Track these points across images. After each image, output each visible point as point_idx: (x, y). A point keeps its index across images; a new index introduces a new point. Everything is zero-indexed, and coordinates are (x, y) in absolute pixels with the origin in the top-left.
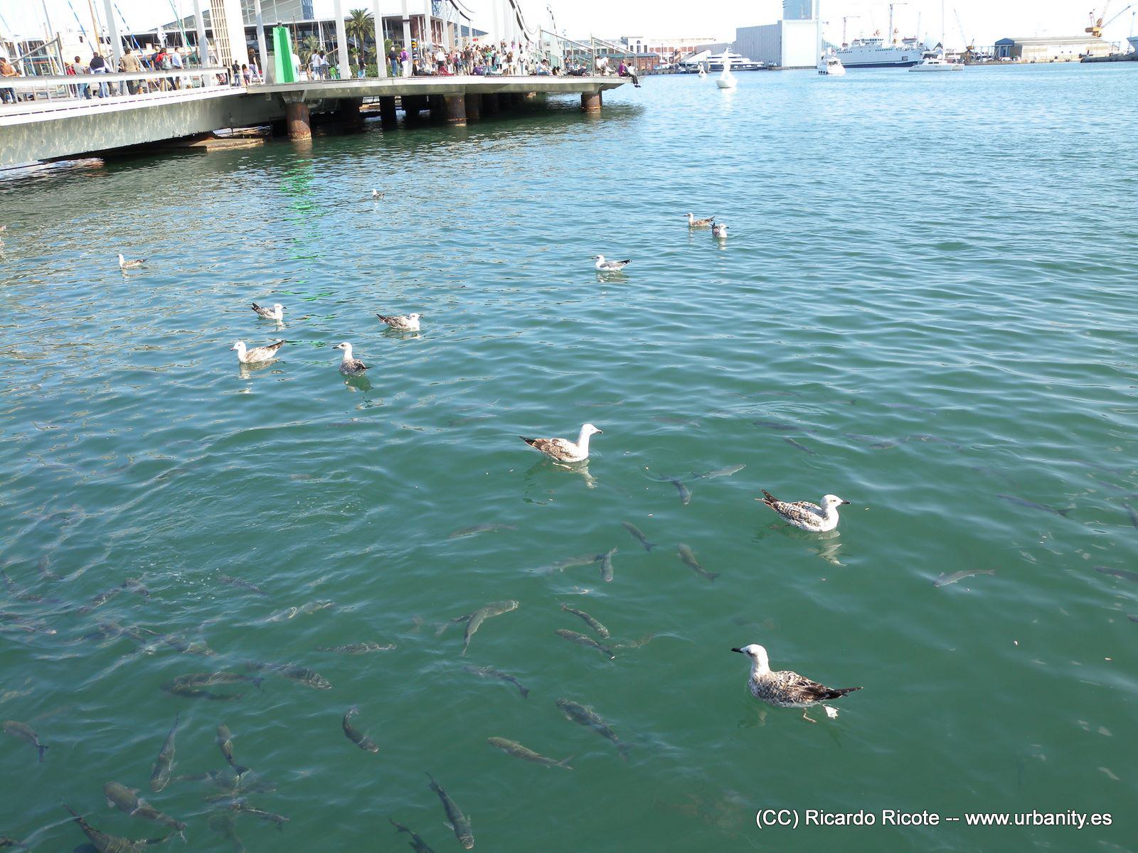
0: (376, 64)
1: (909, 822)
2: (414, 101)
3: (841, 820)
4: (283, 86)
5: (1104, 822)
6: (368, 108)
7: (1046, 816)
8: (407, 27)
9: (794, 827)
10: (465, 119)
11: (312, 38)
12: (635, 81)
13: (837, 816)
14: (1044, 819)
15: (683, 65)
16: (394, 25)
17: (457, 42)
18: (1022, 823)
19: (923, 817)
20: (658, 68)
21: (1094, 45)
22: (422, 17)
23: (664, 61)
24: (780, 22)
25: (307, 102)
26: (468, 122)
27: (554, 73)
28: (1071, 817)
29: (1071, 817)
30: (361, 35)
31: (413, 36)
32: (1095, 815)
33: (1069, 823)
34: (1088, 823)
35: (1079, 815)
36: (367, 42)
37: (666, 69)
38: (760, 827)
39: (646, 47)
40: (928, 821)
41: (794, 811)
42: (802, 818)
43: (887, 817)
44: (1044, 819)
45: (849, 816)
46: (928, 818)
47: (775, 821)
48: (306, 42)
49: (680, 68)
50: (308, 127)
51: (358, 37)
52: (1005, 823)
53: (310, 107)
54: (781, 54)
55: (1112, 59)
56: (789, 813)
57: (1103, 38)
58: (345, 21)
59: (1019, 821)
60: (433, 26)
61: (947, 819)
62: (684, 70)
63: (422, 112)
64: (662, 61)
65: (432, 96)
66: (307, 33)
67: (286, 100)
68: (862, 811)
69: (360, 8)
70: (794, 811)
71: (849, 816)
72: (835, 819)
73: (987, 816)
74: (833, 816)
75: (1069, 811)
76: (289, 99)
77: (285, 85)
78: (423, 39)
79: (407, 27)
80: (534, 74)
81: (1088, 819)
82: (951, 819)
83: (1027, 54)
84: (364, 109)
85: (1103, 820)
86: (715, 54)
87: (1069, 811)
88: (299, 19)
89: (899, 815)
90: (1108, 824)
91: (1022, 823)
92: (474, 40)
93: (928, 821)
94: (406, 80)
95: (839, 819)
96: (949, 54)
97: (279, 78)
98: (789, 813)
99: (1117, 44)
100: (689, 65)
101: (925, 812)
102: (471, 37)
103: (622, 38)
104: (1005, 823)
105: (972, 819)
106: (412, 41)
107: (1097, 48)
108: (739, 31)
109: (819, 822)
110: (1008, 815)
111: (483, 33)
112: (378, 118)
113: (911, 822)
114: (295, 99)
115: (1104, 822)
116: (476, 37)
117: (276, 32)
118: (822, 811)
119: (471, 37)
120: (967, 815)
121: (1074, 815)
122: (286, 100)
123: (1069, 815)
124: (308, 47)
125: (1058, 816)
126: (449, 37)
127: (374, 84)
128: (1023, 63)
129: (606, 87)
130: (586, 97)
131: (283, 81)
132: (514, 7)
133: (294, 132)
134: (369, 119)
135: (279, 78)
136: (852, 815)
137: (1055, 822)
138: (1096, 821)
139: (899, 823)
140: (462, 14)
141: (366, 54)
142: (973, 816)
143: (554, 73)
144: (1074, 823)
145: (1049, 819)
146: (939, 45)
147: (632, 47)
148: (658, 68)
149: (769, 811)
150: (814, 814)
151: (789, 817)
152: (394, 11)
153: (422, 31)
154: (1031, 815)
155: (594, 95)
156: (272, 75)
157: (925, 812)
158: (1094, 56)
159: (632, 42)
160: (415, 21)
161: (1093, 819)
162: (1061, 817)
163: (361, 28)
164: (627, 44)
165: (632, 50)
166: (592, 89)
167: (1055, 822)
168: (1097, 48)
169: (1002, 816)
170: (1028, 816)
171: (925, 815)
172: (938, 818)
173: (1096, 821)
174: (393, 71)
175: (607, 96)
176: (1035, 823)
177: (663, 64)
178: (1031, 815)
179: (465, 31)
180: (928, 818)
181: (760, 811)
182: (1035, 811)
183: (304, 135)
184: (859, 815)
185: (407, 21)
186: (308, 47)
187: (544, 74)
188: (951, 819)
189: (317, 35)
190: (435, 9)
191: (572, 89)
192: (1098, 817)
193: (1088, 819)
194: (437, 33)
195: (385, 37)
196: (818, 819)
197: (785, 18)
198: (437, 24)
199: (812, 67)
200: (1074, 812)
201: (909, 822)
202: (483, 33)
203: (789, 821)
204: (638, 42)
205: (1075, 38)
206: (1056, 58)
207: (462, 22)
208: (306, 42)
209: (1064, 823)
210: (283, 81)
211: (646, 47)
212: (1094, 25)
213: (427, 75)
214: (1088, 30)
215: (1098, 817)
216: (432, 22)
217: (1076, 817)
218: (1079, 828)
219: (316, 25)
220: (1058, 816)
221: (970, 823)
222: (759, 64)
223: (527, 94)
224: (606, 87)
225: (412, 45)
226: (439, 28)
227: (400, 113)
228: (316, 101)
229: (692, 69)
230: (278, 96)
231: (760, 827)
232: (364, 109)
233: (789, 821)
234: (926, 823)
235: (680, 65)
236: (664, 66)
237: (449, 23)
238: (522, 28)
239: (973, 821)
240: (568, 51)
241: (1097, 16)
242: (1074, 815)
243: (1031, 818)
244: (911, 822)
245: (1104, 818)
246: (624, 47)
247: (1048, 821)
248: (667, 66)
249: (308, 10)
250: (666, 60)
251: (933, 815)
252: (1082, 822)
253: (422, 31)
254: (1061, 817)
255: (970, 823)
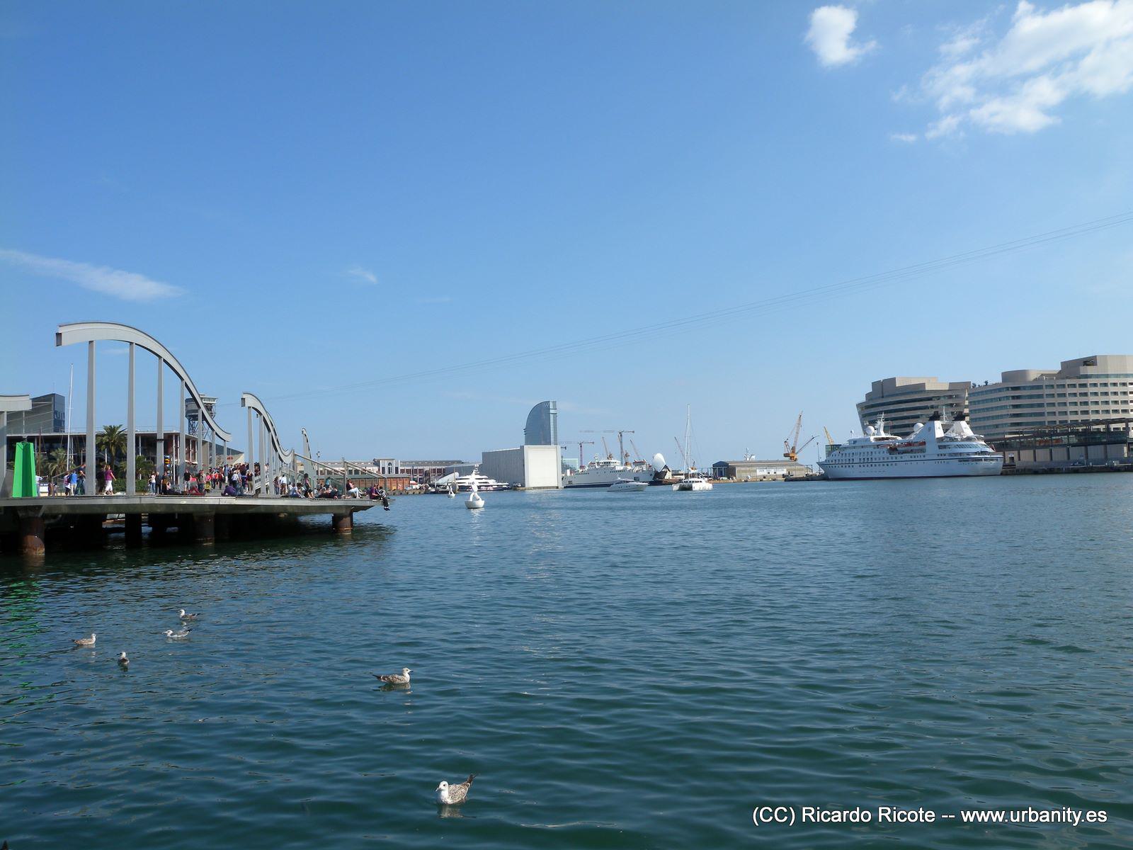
0: (125, 478)
1: (905, 819)
2: (161, 519)
3: (838, 817)
4: (20, 501)
5: (1099, 819)
6: (113, 523)
7: (1041, 813)
8: (160, 447)
9: (791, 825)
10: (214, 538)
11: (60, 450)
12: (385, 503)
13: (833, 813)
14: (1040, 816)
15: (433, 486)
16: (147, 442)
17: (211, 460)
18: (1018, 820)
19: (919, 814)
20: (409, 489)
21: (793, 467)
22: (177, 435)
23: (414, 482)
24: (522, 448)
25: (45, 517)
26: (216, 541)
27: (306, 495)
28: (1066, 814)
29: (1066, 814)
30: (113, 449)
31: (166, 452)
32: (1090, 812)
33: (1064, 821)
34: (1083, 821)
35: (1074, 812)
36: (119, 457)
37: (417, 489)
38: (757, 825)
39: (397, 469)
40: (924, 818)
41: (791, 808)
42: (799, 814)
43: (883, 814)
44: (1040, 816)
45: (845, 813)
46: (924, 815)
47: (771, 818)
48: (53, 454)
49: (430, 488)
50: (41, 542)
51: (110, 451)
52: (1001, 820)
53: (47, 522)
54: (524, 465)
55: (809, 478)
56: (785, 810)
57: (798, 462)
58: (97, 436)
59: (1015, 818)
60: (188, 445)
61: (943, 816)
62: (433, 490)
63: (170, 529)
64: (411, 482)
65: (180, 515)
66: (55, 445)
67: (21, 514)
68: (858, 808)
69: (115, 424)
70: (791, 808)
71: (845, 813)
72: (831, 816)
73: (983, 813)
74: (829, 813)
75: (1064, 808)
76: (24, 514)
77: (21, 499)
78: (176, 456)
79: (160, 447)
80: (286, 497)
81: (1083, 816)
82: (947, 816)
83: (741, 474)
84: (107, 524)
85: (1098, 817)
86: (463, 475)
87: (1064, 808)
88: (49, 432)
89: (895, 812)
90: (1104, 821)
91: (1018, 820)
92: (229, 459)
93: (924, 818)
94: (152, 499)
95: (836, 816)
96: (675, 475)
97: (17, 492)
98: (785, 810)
99: (810, 467)
100: (439, 486)
101: (921, 809)
102: (226, 456)
103: (374, 460)
104: (1001, 820)
105: (967, 817)
106: (165, 458)
107: (795, 470)
108: (485, 455)
109: (816, 819)
110: (1003, 812)
111: (239, 453)
112: (122, 535)
113: (907, 820)
114: (31, 514)
115: (1099, 819)
116: (231, 456)
117: (19, 447)
118: (818, 808)
119: (226, 456)
120: (962, 812)
121: (1069, 812)
122: (20, 515)
123: (1064, 812)
124: (55, 459)
125: (1053, 813)
126: (204, 455)
127: (119, 497)
128: (738, 482)
129: (357, 509)
130: (337, 519)
131: (20, 496)
132: (269, 430)
133: (25, 548)
134: (113, 535)
135: (17, 492)
136: (848, 812)
137: (1050, 819)
138: (1091, 818)
139: (895, 821)
140: (218, 435)
141: (116, 468)
142: (968, 813)
143: (306, 495)
144: (1069, 820)
145: (1044, 816)
146: (666, 467)
147: (383, 468)
148: (409, 489)
149: (766, 808)
150: (811, 811)
151: (785, 814)
152: (149, 428)
153: (177, 448)
154: (1027, 812)
155: (346, 517)
156: (8, 488)
157: (921, 809)
158: (794, 477)
159: (384, 464)
160: (169, 439)
161: (1088, 816)
162: (1056, 815)
163: (113, 444)
164: (379, 466)
165: (383, 472)
166: (343, 511)
167: (1050, 819)
168: (795, 470)
169: (997, 813)
170: (1024, 813)
171: (921, 812)
172: (934, 815)
173: (1091, 818)
174: (142, 489)
175: (358, 517)
176: (1030, 820)
177: (414, 484)
178: (1027, 812)
179: (220, 450)
180: (924, 815)
181: (757, 808)
182: (1030, 809)
183: (37, 550)
184: (855, 812)
185: (161, 440)
186: (55, 459)
187: (296, 496)
188: (947, 816)
189: (65, 447)
190: (192, 428)
191: (322, 510)
192: (1093, 814)
193: (1083, 816)
194: (192, 451)
195: (137, 453)
196: (815, 816)
197: (527, 444)
198: (191, 442)
199: (553, 487)
200: (1069, 809)
201: (905, 819)
202: (239, 453)
203: (786, 818)
204: (390, 464)
205: (777, 461)
206: (765, 477)
207: (219, 442)
208: (53, 454)
209: (1059, 820)
210: (20, 496)
211: (397, 469)
212: (790, 451)
213: (177, 494)
214: (786, 455)
215: (1093, 814)
216: (188, 440)
217: (1071, 814)
218: (1074, 825)
219: (66, 438)
220: (1053, 813)
221: (965, 820)
222: (505, 485)
223: (279, 514)
224: (357, 509)
225: (165, 461)
226: (194, 447)
227: (146, 529)
228: (55, 516)
229: (441, 490)
230: (12, 511)
231: (757, 825)
232: (107, 524)
233: (786, 818)
234: (922, 820)
235: (430, 486)
236: (414, 487)
237: (204, 442)
238: (276, 450)
239: (968, 818)
240: (321, 471)
241: (791, 445)
242: (1069, 812)
243: (1027, 815)
244: (907, 820)
245: (1099, 815)
246: (376, 469)
247: (1044, 819)
248: (418, 486)
249: (59, 424)
250: (416, 482)
251: (929, 812)
252: (1077, 819)
253: (177, 448)
254: (1056, 815)
255: (965, 820)
